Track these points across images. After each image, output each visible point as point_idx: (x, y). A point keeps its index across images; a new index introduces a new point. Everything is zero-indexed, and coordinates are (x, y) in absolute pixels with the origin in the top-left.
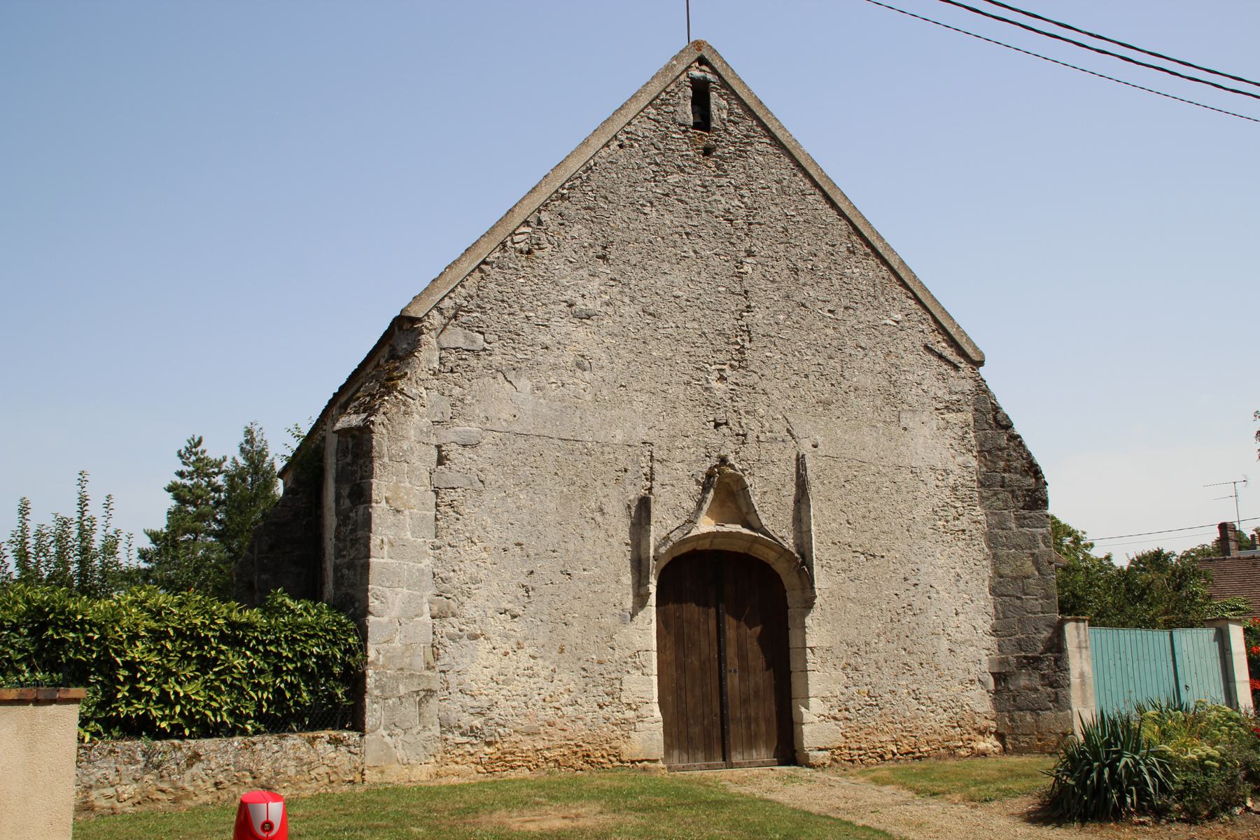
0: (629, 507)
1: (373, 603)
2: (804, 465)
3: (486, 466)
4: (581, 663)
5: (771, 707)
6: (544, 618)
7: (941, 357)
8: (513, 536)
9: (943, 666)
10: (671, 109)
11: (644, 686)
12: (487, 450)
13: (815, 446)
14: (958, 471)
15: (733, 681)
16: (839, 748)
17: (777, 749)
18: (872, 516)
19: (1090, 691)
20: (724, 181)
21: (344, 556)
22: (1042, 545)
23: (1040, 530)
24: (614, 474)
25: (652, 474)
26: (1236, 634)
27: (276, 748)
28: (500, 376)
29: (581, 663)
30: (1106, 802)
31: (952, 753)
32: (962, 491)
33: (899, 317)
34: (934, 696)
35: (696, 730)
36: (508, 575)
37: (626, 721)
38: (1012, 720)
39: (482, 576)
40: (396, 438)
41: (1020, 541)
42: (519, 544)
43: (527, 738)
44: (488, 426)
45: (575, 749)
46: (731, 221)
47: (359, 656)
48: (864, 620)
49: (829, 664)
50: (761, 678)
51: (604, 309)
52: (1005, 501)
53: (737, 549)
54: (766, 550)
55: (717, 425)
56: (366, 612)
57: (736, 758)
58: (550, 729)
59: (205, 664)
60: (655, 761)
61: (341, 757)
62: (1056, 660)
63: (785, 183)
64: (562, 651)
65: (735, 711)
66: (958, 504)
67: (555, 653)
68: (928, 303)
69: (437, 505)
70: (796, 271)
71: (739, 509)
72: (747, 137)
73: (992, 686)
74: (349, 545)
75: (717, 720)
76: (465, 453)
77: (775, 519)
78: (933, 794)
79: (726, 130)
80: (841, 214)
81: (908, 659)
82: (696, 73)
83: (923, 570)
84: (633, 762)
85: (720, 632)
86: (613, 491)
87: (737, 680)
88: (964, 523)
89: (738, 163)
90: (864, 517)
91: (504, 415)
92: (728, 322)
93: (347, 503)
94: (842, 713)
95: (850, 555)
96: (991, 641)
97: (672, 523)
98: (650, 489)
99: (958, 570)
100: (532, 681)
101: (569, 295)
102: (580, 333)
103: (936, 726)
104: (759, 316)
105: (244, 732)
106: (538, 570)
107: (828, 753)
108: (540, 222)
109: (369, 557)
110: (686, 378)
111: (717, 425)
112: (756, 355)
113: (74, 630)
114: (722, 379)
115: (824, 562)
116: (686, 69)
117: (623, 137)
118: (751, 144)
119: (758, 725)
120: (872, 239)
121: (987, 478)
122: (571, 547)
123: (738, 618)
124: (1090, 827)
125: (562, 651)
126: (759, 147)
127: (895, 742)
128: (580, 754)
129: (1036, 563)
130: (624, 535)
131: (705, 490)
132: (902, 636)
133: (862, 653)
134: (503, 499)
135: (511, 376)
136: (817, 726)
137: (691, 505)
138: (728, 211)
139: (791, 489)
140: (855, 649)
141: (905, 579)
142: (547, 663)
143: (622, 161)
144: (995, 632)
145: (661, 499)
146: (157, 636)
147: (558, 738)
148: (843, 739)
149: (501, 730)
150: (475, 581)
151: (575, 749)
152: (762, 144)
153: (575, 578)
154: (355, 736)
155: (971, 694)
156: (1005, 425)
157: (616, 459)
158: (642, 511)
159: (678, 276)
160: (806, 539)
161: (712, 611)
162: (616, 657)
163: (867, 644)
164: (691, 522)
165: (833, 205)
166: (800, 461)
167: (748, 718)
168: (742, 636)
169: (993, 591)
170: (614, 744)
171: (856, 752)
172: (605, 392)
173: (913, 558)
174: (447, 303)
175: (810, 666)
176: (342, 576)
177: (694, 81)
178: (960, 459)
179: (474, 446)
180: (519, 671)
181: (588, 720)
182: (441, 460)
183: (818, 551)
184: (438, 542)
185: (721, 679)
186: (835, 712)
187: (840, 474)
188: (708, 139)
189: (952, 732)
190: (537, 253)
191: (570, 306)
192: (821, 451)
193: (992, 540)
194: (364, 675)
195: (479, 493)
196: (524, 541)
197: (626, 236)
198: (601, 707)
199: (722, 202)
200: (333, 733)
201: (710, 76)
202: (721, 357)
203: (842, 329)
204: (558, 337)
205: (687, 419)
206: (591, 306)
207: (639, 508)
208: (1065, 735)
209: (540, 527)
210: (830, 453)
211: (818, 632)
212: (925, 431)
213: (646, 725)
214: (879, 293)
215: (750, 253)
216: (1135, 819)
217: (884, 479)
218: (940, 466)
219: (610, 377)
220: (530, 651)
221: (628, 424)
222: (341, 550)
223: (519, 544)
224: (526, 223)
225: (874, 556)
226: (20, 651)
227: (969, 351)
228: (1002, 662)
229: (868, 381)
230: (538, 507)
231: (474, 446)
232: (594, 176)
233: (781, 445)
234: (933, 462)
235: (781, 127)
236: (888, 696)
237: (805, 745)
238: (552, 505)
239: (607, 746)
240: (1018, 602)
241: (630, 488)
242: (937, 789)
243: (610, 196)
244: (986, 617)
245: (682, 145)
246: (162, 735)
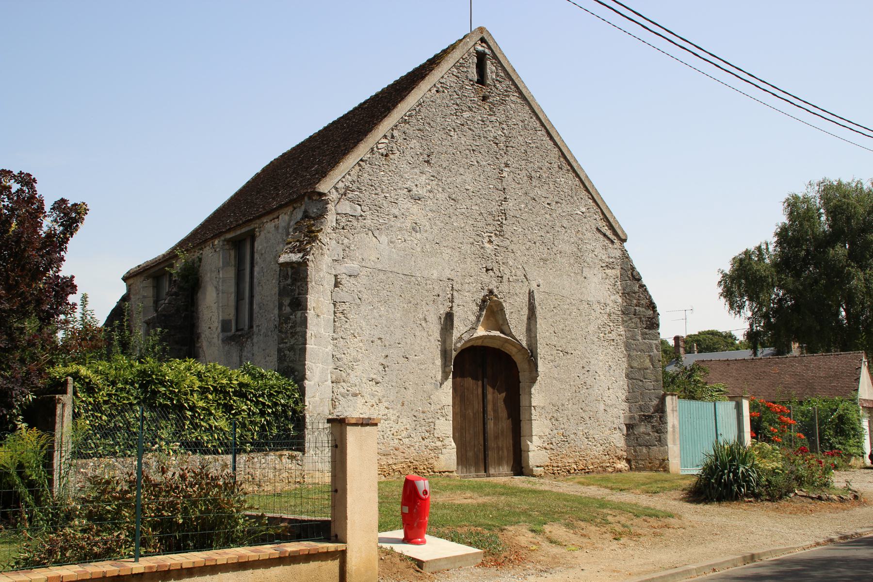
1: (308, 373)
2: (533, 297)
3: (363, 289)
6: (394, 384)
7: (605, 235)
8: (377, 333)
9: (601, 419)
10: (465, 70)
11: (445, 427)
12: (363, 280)
14: (611, 304)
15: (491, 425)
19: (677, 436)
20: (493, 118)
21: (286, 343)
22: (655, 350)
23: (655, 342)
26: (746, 404)
27: (263, 461)
28: (370, 233)
29: (413, 412)
30: (732, 490)
31: (605, 469)
32: (613, 317)
33: (584, 210)
34: (596, 437)
35: (470, 454)
37: (436, 448)
38: (635, 451)
39: (360, 356)
40: (318, 271)
41: (643, 347)
46: (497, 144)
47: (300, 405)
49: (543, 416)
50: (505, 424)
51: (427, 195)
52: (636, 324)
54: (511, 347)
55: (487, 270)
56: (303, 378)
57: (492, 471)
58: (396, 452)
59: (228, 408)
61: (292, 466)
62: (661, 417)
63: (526, 122)
64: (403, 405)
65: (491, 444)
66: (611, 324)
68: (599, 202)
69: (335, 312)
70: (531, 178)
71: (497, 321)
72: (506, 91)
73: (625, 432)
74: (289, 335)
75: (482, 448)
78: (621, 490)
79: (495, 86)
80: (556, 144)
81: (583, 415)
82: (480, 48)
83: (593, 362)
86: (432, 308)
88: (613, 335)
89: (501, 108)
91: (373, 258)
92: (494, 208)
93: (287, 310)
96: (625, 406)
98: (451, 308)
101: (409, 184)
102: (415, 209)
103: (597, 454)
104: (511, 204)
105: (245, 451)
106: (390, 355)
108: (393, 137)
109: (306, 344)
110: (471, 240)
111: (487, 270)
112: (509, 228)
113: (164, 386)
114: (490, 242)
116: (474, 45)
117: (439, 86)
118: (508, 96)
120: (571, 161)
121: (627, 309)
122: (409, 341)
123: (493, 387)
124: (725, 504)
125: (403, 405)
126: (513, 98)
127: (576, 463)
129: (651, 360)
130: (437, 335)
134: (372, 310)
135: (376, 233)
136: (536, 454)
137: (473, 318)
138: (495, 138)
139: (525, 311)
143: (438, 101)
144: (627, 400)
146: (203, 391)
150: (356, 360)
152: (514, 97)
153: (410, 360)
154: (300, 454)
155: (615, 436)
156: (637, 278)
158: (448, 319)
159: (468, 177)
160: (533, 341)
161: (480, 383)
163: (563, 405)
164: (474, 329)
165: (552, 138)
166: (531, 294)
167: (498, 447)
168: (496, 398)
169: (627, 376)
170: (430, 461)
172: (428, 246)
173: (587, 355)
174: (341, 185)
175: (533, 417)
176: (285, 355)
177: (478, 52)
178: (613, 297)
179: (355, 276)
182: (337, 284)
183: (541, 350)
184: (335, 336)
185: (484, 424)
186: (545, 445)
188: (486, 91)
189: (604, 458)
190: (391, 156)
191: (409, 191)
192: (541, 289)
193: (628, 346)
194: (304, 417)
196: (382, 336)
197: (440, 149)
199: (494, 131)
200: (290, 452)
201: (487, 51)
202: (490, 228)
203: (554, 215)
204: (403, 211)
205: (473, 266)
206: (422, 192)
207: (446, 318)
208: (664, 460)
209: (392, 328)
211: (539, 397)
212: (595, 280)
214: (574, 195)
215: (507, 165)
216: (746, 499)
218: (602, 301)
219: (430, 237)
220: (386, 404)
221: (440, 267)
222: (283, 339)
224: (385, 137)
226: (136, 398)
227: (620, 232)
228: (631, 418)
229: (567, 248)
230: (391, 316)
231: (355, 276)
232: (423, 110)
235: (525, 87)
236: (572, 436)
238: (399, 315)
239: (426, 463)
240: (641, 383)
241: (441, 306)
242: (622, 488)
243: (432, 123)
244: (623, 391)
245: (470, 92)
246: (206, 452)
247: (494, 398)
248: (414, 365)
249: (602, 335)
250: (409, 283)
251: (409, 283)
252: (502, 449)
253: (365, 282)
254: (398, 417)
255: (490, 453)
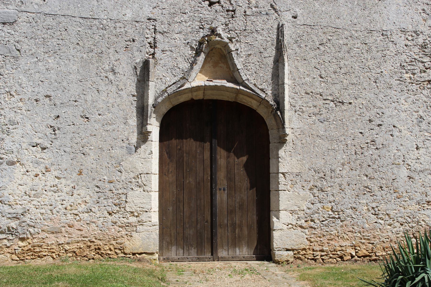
0: (135, 68)
4: (95, 182)
5: (253, 217)
6: (67, 149)
8: (43, 90)
11: (149, 201)
12: (23, 27)
13: (295, 17)
15: (222, 197)
16: (304, 249)
17: (256, 248)
18: (343, 71)
24: (124, 44)
25: (155, 43)
29: (95, 182)
34: (392, 213)
35: (191, 232)
36: (39, 119)
37: (129, 225)
39: (18, 118)
42: (47, 96)
43: (52, 236)
44: (23, 8)
45: (89, 244)
48: (331, 153)
49: (299, 186)
50: (246, 194)
53: (225, 98)
54: (250, 100)
57: (222, 253)
60: (152, 254)
64: (80, 173)
65: (222, 218)
67: (75, 175)
76: (5, 29)
77: (254, 74)
81: (369, 183)
83: (388, 113)
84: (134, 254)
85: (213, 160)
86: (124, 57)
87: (225, 197)
90: (335, 72)
94: (308, 222)
95: (321, 102)
97: (170, 79)
99: (421, 113)
100: (56, 195)
103: (393, 237)
106: (63, 115)
107: (291, 253)
115: (297, 108)
119: (241, 230)
122: (89, 98)
123: (228, 150)
125: (80, 173)
127: (354, 247)
128: (93, 247)
131: (198, 54)
132: (365, 165)
133: (328, 178)
134: (35, 63)
136: (284, 232)
137: (187, 66)
139: (272, 52)
140: (322, 175)
141: (370, 121)
142: (69, 182)
145: (161, 62)
147: (76, 235)
148: (308, 243)
149: (31, 230)
150: (13, 123)
151: (89, 244)
153: (92, 120)
157: (126, 32)
158: (144, 73)
162: (123, 178)
163: (332, 171)
167: (234, 226)
168: (230, 165)
170: (119, 241)
171: (318, 253)
173: (379, 104)
175: (281, 187)
179: (11, 24)
180: (47, 188)
181: (100, 223)
185: (212, 195)
186: (302, 222)
187: (315, 39)
195: (16, 58)
196: (52, 94)
198: (110, 214)
209: (65, 84)
210: (308, 22)
211: (287, 161)
213: (145, 227)
217: (356, 41)
218: (410, 28)
220: (56, 173)
223: (47, 96)
225: (343, 103)
230: (63, 68)
231: (11, 24)
233: (265, 17)
234: (403, 26)
236: (349, 212)
237: (275, 246)
238: (75, 67)
239: (114, 242)
241: (136, 54)
247: (228, 163)
248: (97, 126)
249: (406, 76)
250: (90, 28)
251: (90, 28)
252: (241, 227)
253: (25, 29)
254: (74, 188)
255: (220, 231)
